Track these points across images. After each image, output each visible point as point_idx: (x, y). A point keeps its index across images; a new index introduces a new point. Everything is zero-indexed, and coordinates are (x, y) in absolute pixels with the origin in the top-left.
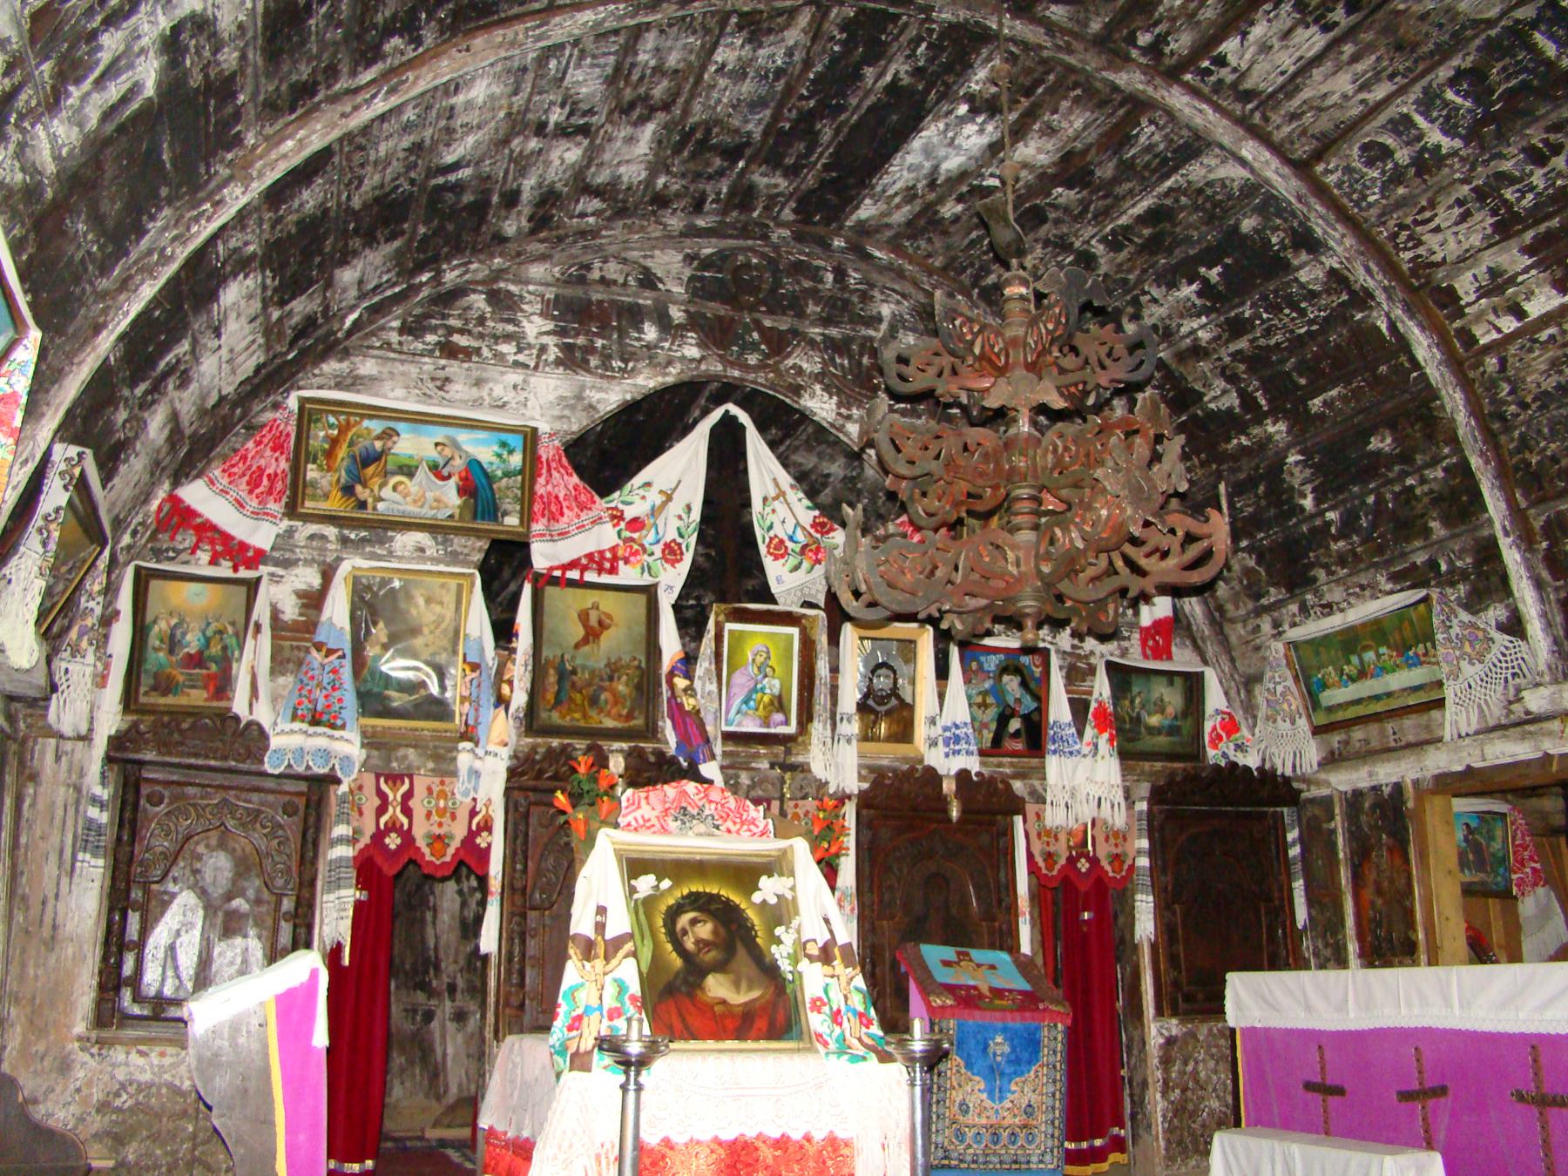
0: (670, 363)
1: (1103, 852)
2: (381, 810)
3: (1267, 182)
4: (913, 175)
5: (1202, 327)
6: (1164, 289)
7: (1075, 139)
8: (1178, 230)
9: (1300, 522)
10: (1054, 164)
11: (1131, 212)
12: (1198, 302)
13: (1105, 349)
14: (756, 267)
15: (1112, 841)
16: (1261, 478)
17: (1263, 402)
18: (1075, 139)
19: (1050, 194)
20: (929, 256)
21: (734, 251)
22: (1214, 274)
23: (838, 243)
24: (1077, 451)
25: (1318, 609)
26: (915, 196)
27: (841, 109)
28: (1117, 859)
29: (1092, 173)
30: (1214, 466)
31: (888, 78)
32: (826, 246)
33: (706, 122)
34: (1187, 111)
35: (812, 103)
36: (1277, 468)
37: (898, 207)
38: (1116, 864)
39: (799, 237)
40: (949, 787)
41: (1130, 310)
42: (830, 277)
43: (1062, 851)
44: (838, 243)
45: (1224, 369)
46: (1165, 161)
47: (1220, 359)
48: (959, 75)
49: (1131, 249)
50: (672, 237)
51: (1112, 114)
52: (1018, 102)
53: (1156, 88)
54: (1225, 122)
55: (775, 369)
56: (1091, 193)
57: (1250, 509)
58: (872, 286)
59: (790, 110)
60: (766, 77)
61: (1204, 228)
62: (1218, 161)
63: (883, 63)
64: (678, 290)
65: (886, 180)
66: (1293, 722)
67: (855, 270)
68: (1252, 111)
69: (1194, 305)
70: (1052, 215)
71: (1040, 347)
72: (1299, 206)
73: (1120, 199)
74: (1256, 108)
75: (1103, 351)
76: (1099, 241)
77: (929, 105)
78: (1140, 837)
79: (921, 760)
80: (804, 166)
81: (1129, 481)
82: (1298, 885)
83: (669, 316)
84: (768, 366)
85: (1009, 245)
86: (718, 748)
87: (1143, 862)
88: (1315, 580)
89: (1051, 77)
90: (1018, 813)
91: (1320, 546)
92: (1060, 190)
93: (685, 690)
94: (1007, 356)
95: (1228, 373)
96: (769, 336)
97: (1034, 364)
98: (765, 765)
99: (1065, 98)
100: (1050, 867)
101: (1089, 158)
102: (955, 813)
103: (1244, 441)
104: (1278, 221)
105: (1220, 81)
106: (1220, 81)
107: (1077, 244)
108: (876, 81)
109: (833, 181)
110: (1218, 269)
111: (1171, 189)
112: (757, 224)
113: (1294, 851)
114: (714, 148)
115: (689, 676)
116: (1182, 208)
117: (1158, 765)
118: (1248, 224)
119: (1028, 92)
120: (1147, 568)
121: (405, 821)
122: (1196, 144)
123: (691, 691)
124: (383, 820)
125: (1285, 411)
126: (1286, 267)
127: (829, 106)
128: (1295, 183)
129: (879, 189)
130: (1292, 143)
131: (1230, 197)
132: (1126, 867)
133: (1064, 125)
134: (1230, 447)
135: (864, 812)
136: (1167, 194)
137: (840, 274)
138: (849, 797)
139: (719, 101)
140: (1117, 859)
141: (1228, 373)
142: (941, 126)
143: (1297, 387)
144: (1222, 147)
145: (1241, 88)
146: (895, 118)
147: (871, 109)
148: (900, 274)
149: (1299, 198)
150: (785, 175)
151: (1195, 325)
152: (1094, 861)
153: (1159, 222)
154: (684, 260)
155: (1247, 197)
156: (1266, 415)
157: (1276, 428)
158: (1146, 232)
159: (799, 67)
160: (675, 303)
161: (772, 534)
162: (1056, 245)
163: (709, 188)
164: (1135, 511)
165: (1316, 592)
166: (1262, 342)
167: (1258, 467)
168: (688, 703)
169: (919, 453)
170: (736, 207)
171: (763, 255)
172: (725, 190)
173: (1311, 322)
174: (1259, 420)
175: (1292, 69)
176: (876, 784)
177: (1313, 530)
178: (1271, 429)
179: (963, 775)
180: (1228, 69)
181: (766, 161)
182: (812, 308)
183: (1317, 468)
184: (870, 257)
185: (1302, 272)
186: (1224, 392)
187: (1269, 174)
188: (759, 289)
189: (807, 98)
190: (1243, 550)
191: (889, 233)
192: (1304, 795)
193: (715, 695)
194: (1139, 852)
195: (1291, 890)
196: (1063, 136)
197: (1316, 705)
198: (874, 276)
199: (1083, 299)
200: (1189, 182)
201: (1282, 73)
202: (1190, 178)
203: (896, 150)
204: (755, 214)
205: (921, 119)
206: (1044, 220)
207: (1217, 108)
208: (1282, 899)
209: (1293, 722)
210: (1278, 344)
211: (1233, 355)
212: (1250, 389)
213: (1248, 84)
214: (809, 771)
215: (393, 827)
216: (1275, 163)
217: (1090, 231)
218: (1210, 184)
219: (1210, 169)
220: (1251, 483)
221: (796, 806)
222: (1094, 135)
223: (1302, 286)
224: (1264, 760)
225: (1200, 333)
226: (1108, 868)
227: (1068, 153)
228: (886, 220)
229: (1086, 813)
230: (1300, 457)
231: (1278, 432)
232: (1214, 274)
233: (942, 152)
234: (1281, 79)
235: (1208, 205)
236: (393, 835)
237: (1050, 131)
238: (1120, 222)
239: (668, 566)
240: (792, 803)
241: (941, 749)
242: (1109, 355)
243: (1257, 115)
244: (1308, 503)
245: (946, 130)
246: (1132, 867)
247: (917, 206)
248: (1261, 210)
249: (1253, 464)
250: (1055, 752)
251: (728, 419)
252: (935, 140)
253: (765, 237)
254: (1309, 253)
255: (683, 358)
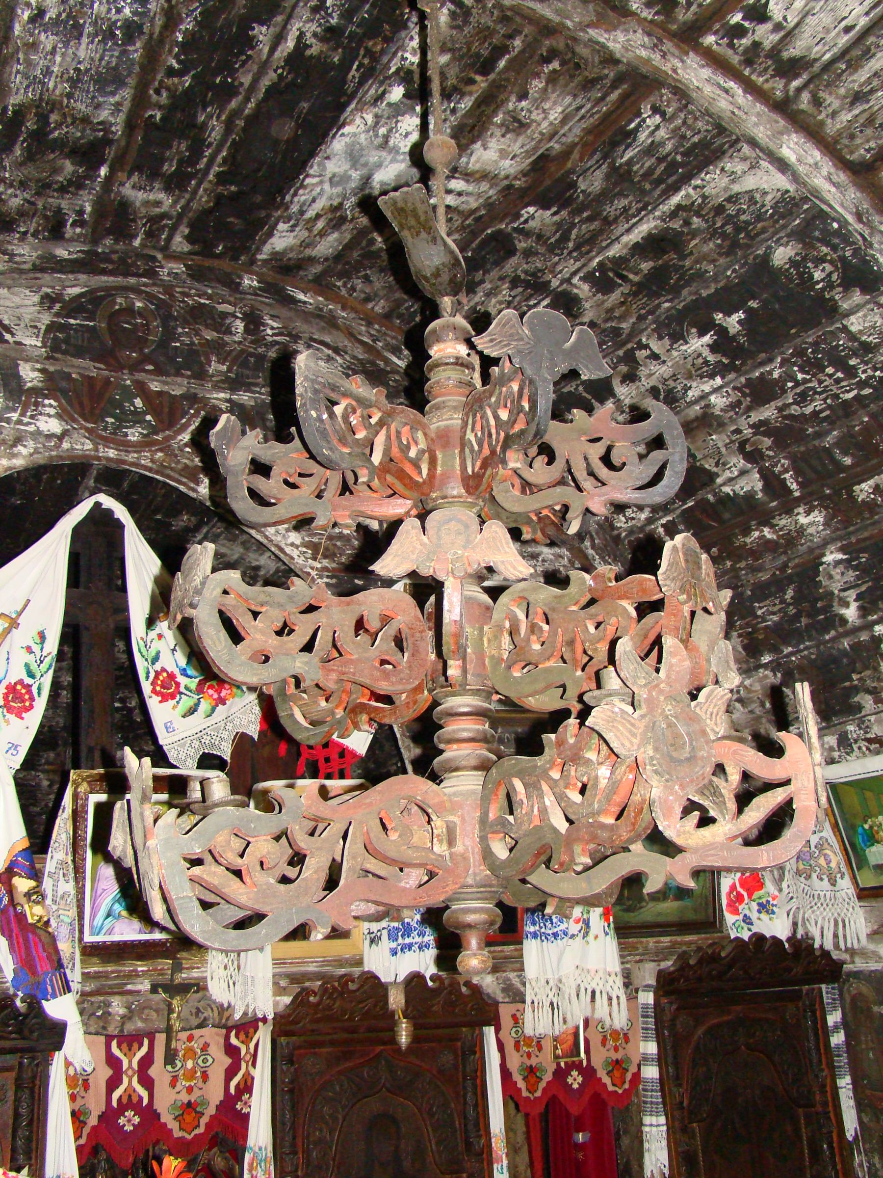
0: (18, 440)
1: (600, 1059)
2: (113, 1083)
3: (816, 193)
4: (338, 190)
5: (716, 390)
6: (667, 341)
7: (552, 136)
8: (687, 263)
9: (840, 636)
10: (525, 174)
11: (625, 239)
12: (711, 358)
13: (598, 450)
14: (141, 313)
15: (611, 1043)
16: (790, 580)
17: (794, 486)
18: (552, 136)
19: (518, 216)
20: (368, 299)
21: (110, 292)
22: (733, 322)
23: (249, 282)
24: (553, 633)
25: (863, 744)
26: (343, 220)
27: (230, 91)
28: (617, 1066)
29: (573, 185)
30: (729, 564)
31: (290, 44)
32: (235, 287)
33: (37, 104)
34: (708, 90)
35: (187, 81)
36: (814, 564)
37: (322, 234)
38: (617, 1074)
39: (197, 274)
40: (396, 1000)
41: (623, 368)
42: (239, 326)
43: (547, 1062)
44: (249, 282)
45: (742, 444)
46: (673, 166)
47: (738, 431)
48: (388, 40)
49: (625, 289)
50: (21, 272)
51: (602, 99)
52: (472, 82)
53: (664, 56)
54: (759, 107)
55: (165, 448)
56: (573, 214)
57: (775, 618)
58: (296, 338)
59: (158, 92)
60: (113, 36)
61: (722, 261)
62: (744, 166)
63: (279, 19)
64: (32, 341)
65: (303, 196)
66: (833, 883)
67: (273, 317)
68: (799, 90)
69: (706, 362)
70: (522, 245)
71: (486, 452)
72: (859, 227)
73: (608, 222)
74: (805, 85)
75: (596, 452)
76: (583, 279)
77: (350, 87)
78: (646, 1039)
79: (359, 962)
80: (192, 176)
81: (652, 727)
82: (845, 1082)
83: (18, 377)
84: (155, 443)
85: (437, 274)
86: (75, 976)
87: (651, 1072)
88: (859, 708)
89: (518, 43)
90: (489, 1024)
91: (866, 668)
92: (531, 210)
93: (28, 895)
94: (433, 462)
95: (748, 448)
96: (153, 401)
97: (478, 477)
98: (145, 986)
99: (537, 75)
100: (531, 1089)
101: (569, 165)
102: (404, 1038)
103: (767, 533)
104: (825, 250)
105: (756, 45)
106: (756, 45)
107: (555, 283)
108: (273, 49)
109: (233, 197)
110: (741, 315)
111: (679, 207)
112: (139, 255)
113: (838, 1039)
114: (60, 145)
115: (36, 875)
116: (694, 234)
117: (666, 940)
118: (782, 255)
119: (486, 68)
120: (679, 841)
121: (144, 1094)
122: (718, 142)
123: (36, 895)
124: (116, 1095)
125: (823, 498)
126: (832, 311)
127: (212, 87)
128: (853, 194)
129: (294, 208)
130: (852, 137)
131: (759, 218)
132: (629, 1076)
133: (536, 116)
134: (748, 540)
135: (283, 1040)
136: (673, 214)
137: (253, 322)
138: (264, 1020)
139: (48, 72)
140: (617, 1066)
141: (748, 448)
142: (369, 118)
143: (840, 467)
144: (753, 143)
145: (785, 55)
146: (305, 105)
147: (271, 91)
148: (331, 322)
149: (859, 216)
150: (167, 189)
151: (707, 388)
152: (588, 1072)
153: (664, 252)
154: (41, 303)
155: (783, 217)
156: (798, 501)
157: (810, 518)
158: (646, 266)
159: (159, 22)
160: (27, 360)
161: (158, 667)
162: (527, 285)
163: (64, 204)
164: (668, 788)
165: (861, 723)
166: (795, 410)
167: (785, 566)
168: (33, 913)
169: (275, 640)
170: (109, 232)
171: (150, 297)
172: (88, 209)
173: (862, 384)
174: (788, 509)
175: (863, 22)
176: (300, 1000)
177: (857, 647)
178: (803, 520)
179: (415, 980)
180: (769, 26)
181: (137, 168)
182: (216, 367)
183: (864, 571)
184: (294, 301)
185: (853, 319)
186: (743, 473)
187: (819, 182)
188: (144, 341)
189: (180, 74)
190: (765, 666)
191: (317, 269)
192: (847, 967)
193: (72, 899)
194: (645, 1059)
195: (835, 1089)
196: (534, 133)
197: (862, 862)
198: (299, 325)
199: (563, 368)
200: (704, 197)
201: (847, 30)
202: (707, 191)
203: (312, 154)
204: (137, 243)
205: (342, 107)
206: (511, 252)
207: (750, 87)
208: (825, 1104)
209: (833, 883)
210: (815, 413)
211: (757, 426)
212: (777, 469)
213: (794, 51)
214: (205, 988)
215: (130, 1103)
216: (827, 166)
217: (572, 265)
218: (732, 199)
219: (734, 178)
220: (776, 585)
221: (190, 1038)
222: (577, 131)
223: (852, 337)
224: (795, 924)
225: (713, 398)
226: (606, 1080)
227: (542, 157)
228: (308, 252)
229: (577, 1012)
230: (840, 556)
231: (811, 524)
232: (733, 322)
233: (373, 157)
234: (844, 40)
235: (729, 229)
236: (129, 1113)
237: (517, 125)
238: (611, 253)
239: (12, 717)
240: (184, 1035)
241: (386, 944)
242: (606, 460)
243: (805, 96)
244: (851, 613)
245: (376, 124)
246: (637, 1076)
247: (345, 234)
248: (802, 235)
249: (779, 562)
250: (535, 935)
251: (99, 515)
252: (363, 138)
253: (151, 273)
254: (865, 290)
255: (38, 432)
